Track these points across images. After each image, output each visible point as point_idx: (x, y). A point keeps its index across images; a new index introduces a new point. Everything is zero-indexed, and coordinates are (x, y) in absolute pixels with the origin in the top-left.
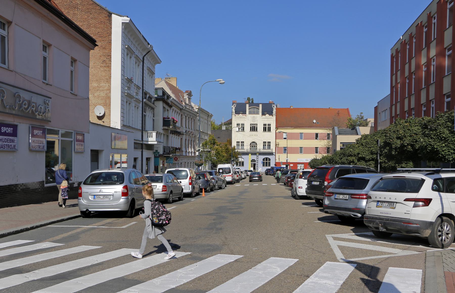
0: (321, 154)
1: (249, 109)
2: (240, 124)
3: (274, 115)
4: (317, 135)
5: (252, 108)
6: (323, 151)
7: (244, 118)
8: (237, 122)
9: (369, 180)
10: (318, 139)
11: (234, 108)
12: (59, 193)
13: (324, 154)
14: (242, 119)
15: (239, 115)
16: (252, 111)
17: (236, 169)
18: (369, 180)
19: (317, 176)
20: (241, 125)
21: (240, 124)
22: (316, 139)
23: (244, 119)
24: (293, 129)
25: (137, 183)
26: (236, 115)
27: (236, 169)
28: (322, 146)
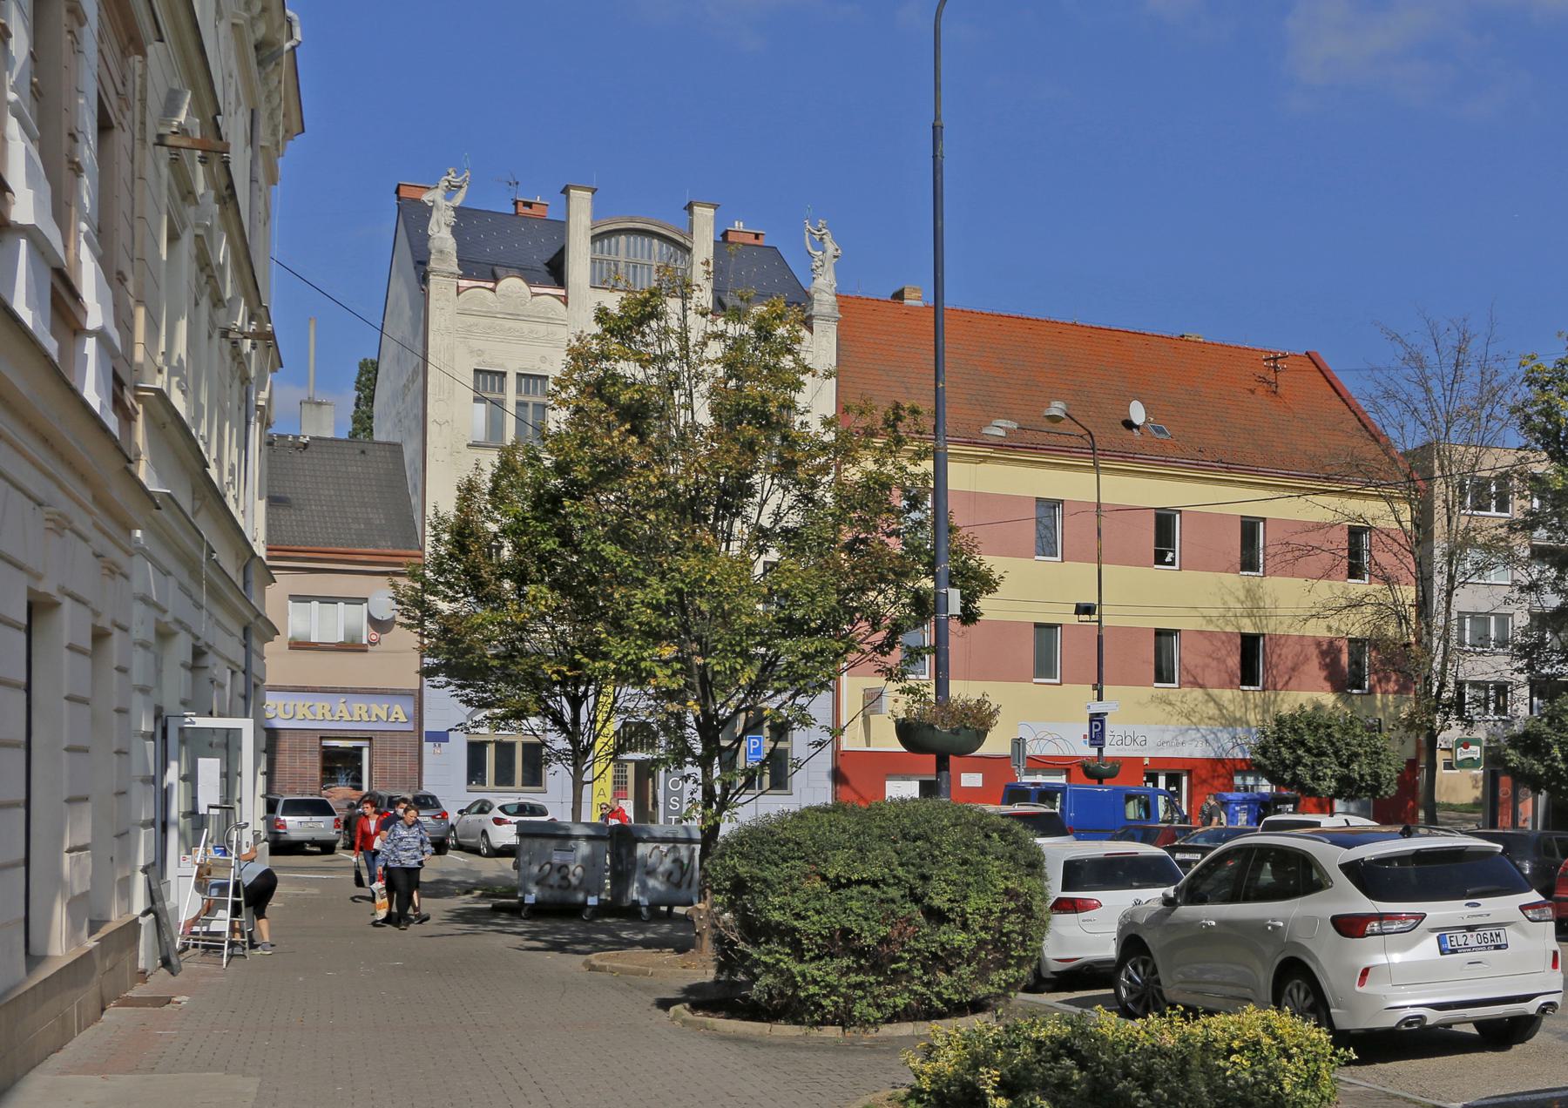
0: (1201, 686)
1: (595, 238)
2: (504, 374)
3: (825, 318)
4: (1164, 523)
5: (623, 238)
6: (1214, 664)
7: (549, 321)
8: (480, 352)
9: (1341, 867)
10: (1172, 563)
11: (450, 217)
12: (1066, 991)
13: (1222, 687)
14: (525, 326)
15: (493, 290)
16: (622, 257)
17: (502, 809)
18: (1341, 867)
19: (650, 809)
20: (519, 391)
21: (504, 374)
22: (1160, 558)
23: (542, 329)
24: (985, 459)
25: (1013, 953)
26: (464, 283)
27: (502, 809)
28: (1209, 620)
